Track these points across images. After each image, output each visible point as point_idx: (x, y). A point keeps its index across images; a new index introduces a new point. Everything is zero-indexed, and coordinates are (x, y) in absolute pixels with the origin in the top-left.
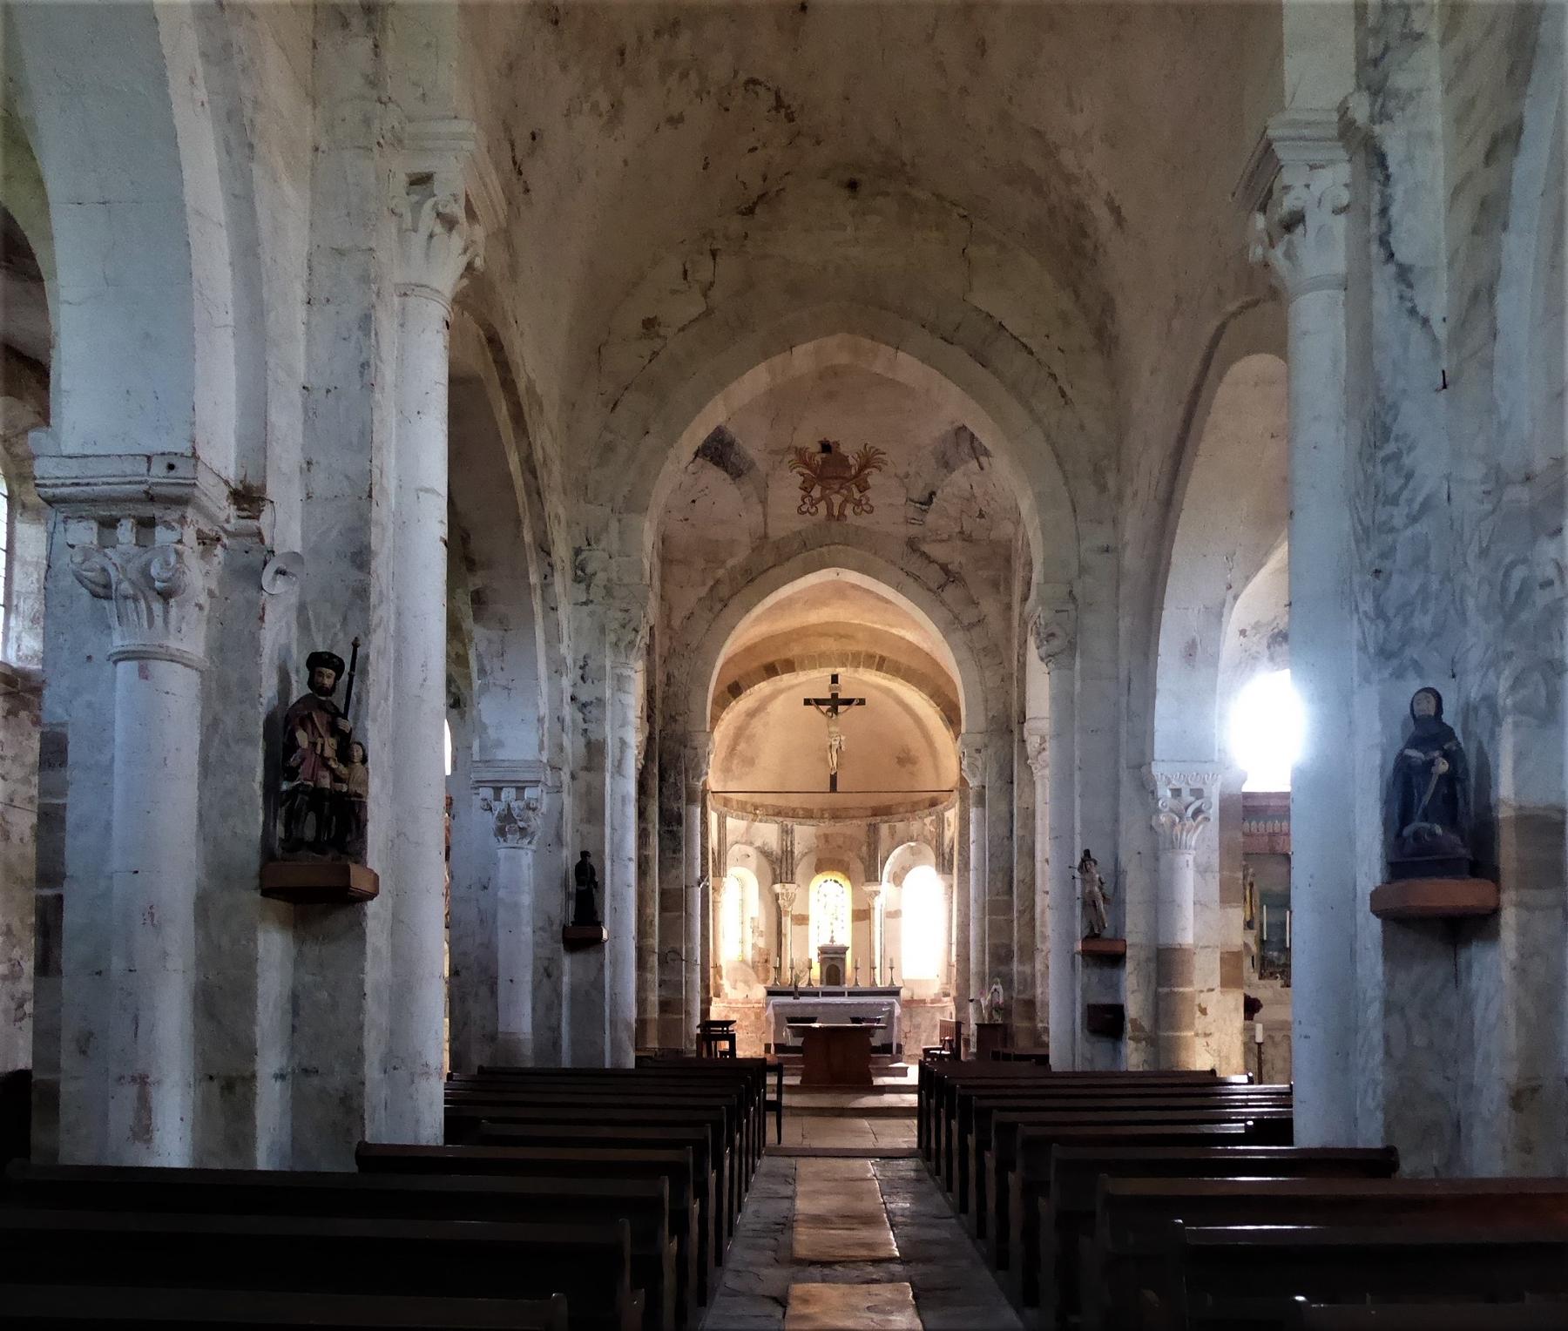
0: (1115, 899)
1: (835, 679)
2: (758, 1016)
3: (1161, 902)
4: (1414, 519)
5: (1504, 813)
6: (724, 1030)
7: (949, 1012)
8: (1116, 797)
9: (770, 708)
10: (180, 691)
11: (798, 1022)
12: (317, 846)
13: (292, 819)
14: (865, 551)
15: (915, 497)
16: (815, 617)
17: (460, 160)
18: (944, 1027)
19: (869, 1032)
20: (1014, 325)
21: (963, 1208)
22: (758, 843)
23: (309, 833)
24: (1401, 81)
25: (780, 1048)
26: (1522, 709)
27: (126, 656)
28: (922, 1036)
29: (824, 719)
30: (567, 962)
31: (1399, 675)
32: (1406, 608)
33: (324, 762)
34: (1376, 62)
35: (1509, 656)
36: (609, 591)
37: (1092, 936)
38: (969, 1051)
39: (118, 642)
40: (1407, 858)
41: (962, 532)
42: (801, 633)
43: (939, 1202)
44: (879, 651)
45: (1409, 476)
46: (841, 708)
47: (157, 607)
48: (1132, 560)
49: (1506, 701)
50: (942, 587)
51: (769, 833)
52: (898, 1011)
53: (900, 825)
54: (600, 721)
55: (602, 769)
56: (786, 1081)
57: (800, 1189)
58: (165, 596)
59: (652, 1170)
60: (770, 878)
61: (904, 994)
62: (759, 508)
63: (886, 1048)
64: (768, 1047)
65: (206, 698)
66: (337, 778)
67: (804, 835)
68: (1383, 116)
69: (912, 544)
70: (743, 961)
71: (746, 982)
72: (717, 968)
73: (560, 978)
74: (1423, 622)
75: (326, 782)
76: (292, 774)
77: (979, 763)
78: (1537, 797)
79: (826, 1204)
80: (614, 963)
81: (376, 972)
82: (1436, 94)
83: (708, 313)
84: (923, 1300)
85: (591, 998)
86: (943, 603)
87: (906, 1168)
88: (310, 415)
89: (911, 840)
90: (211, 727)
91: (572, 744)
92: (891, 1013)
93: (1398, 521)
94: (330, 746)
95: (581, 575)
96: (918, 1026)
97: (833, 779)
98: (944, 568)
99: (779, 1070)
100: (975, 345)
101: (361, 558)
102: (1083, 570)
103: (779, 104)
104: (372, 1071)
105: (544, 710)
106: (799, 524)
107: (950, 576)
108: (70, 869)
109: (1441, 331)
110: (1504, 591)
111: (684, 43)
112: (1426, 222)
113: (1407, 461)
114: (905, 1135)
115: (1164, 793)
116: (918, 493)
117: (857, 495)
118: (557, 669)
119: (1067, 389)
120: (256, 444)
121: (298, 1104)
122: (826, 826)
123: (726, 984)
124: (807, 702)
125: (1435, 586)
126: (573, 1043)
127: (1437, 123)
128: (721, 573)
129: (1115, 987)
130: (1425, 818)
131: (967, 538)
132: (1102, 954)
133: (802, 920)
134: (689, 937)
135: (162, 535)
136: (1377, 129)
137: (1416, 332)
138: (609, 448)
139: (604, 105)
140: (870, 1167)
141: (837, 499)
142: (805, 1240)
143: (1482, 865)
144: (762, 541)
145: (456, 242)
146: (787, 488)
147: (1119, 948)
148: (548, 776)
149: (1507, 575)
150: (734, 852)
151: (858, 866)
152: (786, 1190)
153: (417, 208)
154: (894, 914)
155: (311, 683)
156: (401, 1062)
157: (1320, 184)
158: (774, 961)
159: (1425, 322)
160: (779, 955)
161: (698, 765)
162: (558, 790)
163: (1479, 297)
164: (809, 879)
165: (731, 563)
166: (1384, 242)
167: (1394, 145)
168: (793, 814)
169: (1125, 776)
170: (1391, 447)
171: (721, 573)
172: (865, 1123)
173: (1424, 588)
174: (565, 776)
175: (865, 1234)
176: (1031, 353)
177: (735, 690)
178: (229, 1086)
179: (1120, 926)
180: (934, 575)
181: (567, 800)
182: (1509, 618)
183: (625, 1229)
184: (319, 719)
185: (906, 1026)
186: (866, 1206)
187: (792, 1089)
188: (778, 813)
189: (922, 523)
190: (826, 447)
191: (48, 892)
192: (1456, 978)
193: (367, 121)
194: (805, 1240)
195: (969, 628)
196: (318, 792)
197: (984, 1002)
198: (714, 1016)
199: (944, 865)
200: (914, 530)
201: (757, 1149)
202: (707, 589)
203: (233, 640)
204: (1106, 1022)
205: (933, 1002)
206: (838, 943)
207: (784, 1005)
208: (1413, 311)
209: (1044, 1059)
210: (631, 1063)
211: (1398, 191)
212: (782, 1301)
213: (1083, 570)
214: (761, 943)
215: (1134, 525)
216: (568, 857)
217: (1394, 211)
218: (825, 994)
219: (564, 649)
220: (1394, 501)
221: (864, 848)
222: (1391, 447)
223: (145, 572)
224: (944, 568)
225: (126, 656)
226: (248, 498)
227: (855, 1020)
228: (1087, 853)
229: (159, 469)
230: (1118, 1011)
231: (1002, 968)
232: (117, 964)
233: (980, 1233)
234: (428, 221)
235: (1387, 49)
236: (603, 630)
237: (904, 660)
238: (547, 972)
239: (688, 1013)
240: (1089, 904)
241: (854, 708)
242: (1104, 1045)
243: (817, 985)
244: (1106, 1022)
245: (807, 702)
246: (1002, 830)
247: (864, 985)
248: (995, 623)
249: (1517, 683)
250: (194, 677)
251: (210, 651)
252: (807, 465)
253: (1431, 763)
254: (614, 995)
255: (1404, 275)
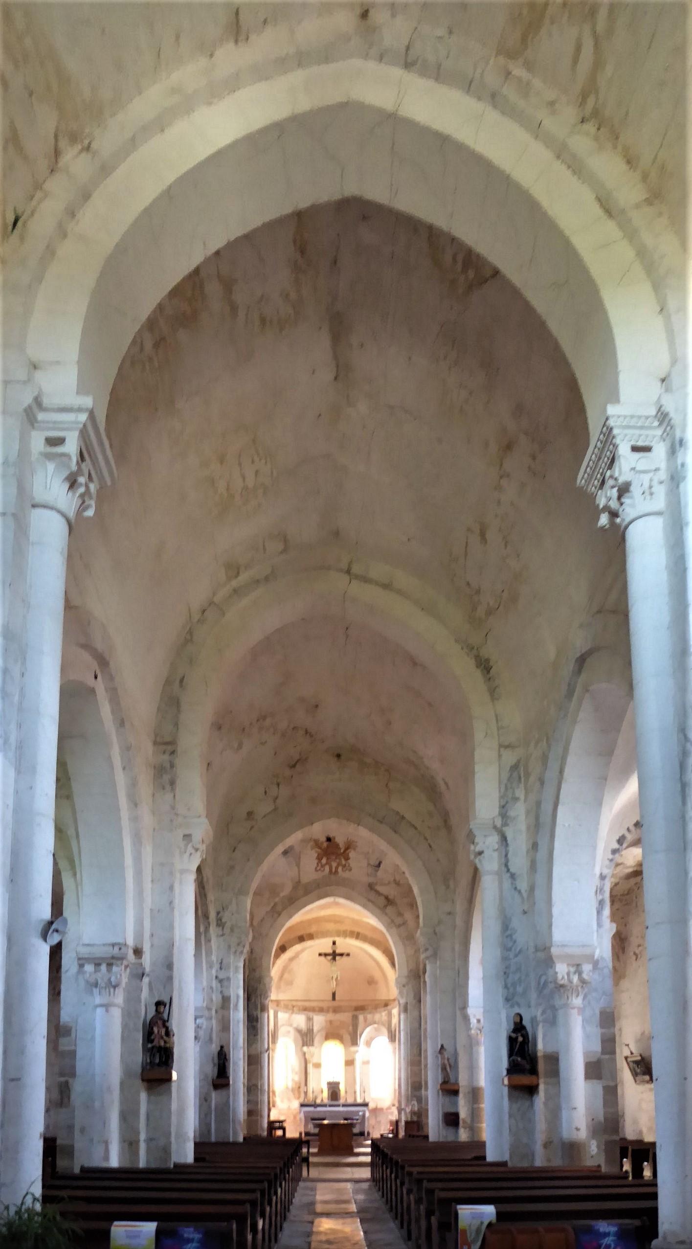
0: (455, 1066)
1: (334, 943)
2: (295, 1117)
3: (472, 1068)
4: (516, 956)
5: (540, 1054)
6: (279, 1125)
7: (394, 1116)
8: (455, 1020)
9: (300, 956)
10: (117, 1014)
11: (314, 1119)
12: (159, 1065)
13: (152, 1056)
14: (348, 889)
15: (372, 863)
16: (323, 913)
17: (202, 830)
18: (391, 1123)
19: (351, 1126)
20: (408, 816)
21: (383, 1196)
22: (295, 1025)
23: (157, 1061)
24: (512, 813)
25: (307, 1134)
26: (545, 1021)
27: (101, 1006)
28: (380, 1129)
29: (329, 964)
30: (214, 1094)
31: (512, 1006)
32: (514, 985)
33: (162, 1038)
34: (503, 807)
35: (540, 1005)
36: (232, 930)
37: (445, 1082)
38: (402, 1133)
39: (98, 1000)
40: (513, 1069)
41: (395, 880)
42: (317, 920)
43: (377, 1195)
44: (357, 930)
45: (515, 942)
46: (337, 958)
47: (112, 990)
48: (459, 921)
49: (539, 1018)
50: (385, 906)
51: (300, 1020)
52: (367, 1114)
53: (369, 1016)
54: (228, 987)
55: (229, 1009)
56: (311, 1150)
57: (319, 1198)
58: (115, 987)
59: (228, 1218)
60: (301, 1042)
61: (372, 1105)
62: (296, 868)
63: (362, 1134)
64: (301, 1134)
65: (123, 1016)
66: (165, 1042)
67: (319, 1021)
68: (505, 824)
69: (371, 886)
70: (287, 1088)
71: (289, 1100)
72: (274, 1093)
73: (211, 1101)
74: (520, 989)
75: (162, 1044)
76: (152, 1041)
77: (405, 991)
78: (550, 1049)
79: (328, 1197)
80: (234, 1095)
81: (174, 1106)
82: (522, 817)
83: (276, 809)
84: (362, 1221)
85: (224, 1111)
86: (386, 914)
87: (365, 1186)
88: (152, 918)
89: (375, 1023)
90: (125, 1027)
91: (216, 998)
92: (364, 1116)
93: (511, 956)
94: (163, 1031)
95: (220, 923)
96: (379, 1122)
97: (334, 995)
98: (387, 898)
99: (308, 1143)
100: (393, 824)
101: (170, 966)
102: (440, 922)
103: (306, 732)
104: (173, 1139)
105: (205, 983)
106: (318, 875)
107: (389, 901)
108: (77, 1074)
109: (525, 895)
110: (539, 983)
111: (268, 722)
112: (519, 862)
113: (514, 937)
114: (366, 1173)
115: (473, 1021)
116: (374, 862)
117: (343, 862)
118: (210, 967)
119: (432, 844)
120: (139, 935)
121: (148, 1150)
122: (331, 1016)
123: (278, 1100)
124: (320, 955)
125: (523, 978)
126: (216, 1130)
127: (523, 827)
128: (277, 900)
129: (456, 1104)
130: (516, 1055)
131: (397, 883)
132: (450, 1090)
133: (318, 1066)
134: (262, 1077)
135: (115, 969)
136: (504, 829)
137: (516, 894)
138: (232, 867)
139: (236, 745)
140: (349, 1185)
141: (334, 865)
142: (319, 1208)
143: (534, 1071)
144: (297, 884)
145: (199, 853)
146: (310, 859)
147: (456, 1088)
148: (206, 1013)
149: (540, 978)
150: (282, 1031)
151: (347, 1037)
152: (313, 1193)
153: (186, 846)
154: (367, 1063)
155: (156, 1010)
156: (181, 1136)
157: (488, 842)
158: (303, 1089)
159: (520, 892)
160: (306, 1084)
161: (266, 992)
162: (211, 1018)
163: (532, 889)
164: (321, 1044)
165: (282, 895)
166: (506, 865)
167: (509, 832)
168: (313, 1010)
169: (458, 1013)
170: (509, 932)
171: (277, 900)
172: (349, 1169)
173: (520, 979)
174: (213, 1012)
175: (343, 1206)
176: (416, 828)
177: (283, 949)
178: (131, 1144)
179: (457, 1079)
180: (382, 901)
181: (214, 1022)
182: (541, 992)
183: (248, 1207)
184: (160, 1023)
185: (372, 1122)
186: (345, 1197)
187: (314, 1155)
188: (305, 1009)
189: (376, 876)
190: (329, 839)
191: (63, 1079)
192: (532, 1105)
193: (171, 821)
194: (319, 1208)
195: (399, 926)
196: (160, 1047)
197: (408, 1110)
198: (272, 1118)
199: (392, 1038)
200: (371, 880)
201: (298, 1179)
202: (270, 907)
203: (132, 998)
204: (452, 1120)
205: (387, 1109)
206: (336, 1080)
207: (309, 1112)
208: (516, 889)
209: (427, 1137)
210: (241, 1139)
211: (511, 849)
212: (312, 1223)
213: (440, 922)
214: (297, 1078)
215: (459, 908)
216: (215, 1048)
217: (509, 856)
218: (330, 1106)
219: (214, 958)
220: (510, 949)
221: (351, 1028)
222: (509, 932)
223: (109, 980)
224: (387, 898)
225: (101, 1006)
226: (138, 952)
227: (346, 1119)
228: (442, 1046)
229: (116, 948)
230: (456, 1116)
231: (417, 1093)
232: (97, 1104)
233: (391, 1209)
234: (190, 849)
235: (507, 802)
236: (229, 947)
237: (369, 934)
238: (204, 1100)
239: (261, 1116)
240: (444, 1069)
241: (345, 958)
242: (451, 1130)
243: (326, 1101)
244: (452, 1120)
245: (320, 955)
246: (417, 1025)
247: (350, 1101)
248: (411, 923)
249: (544, 1012)
250: (120, 1010)
251: (124, 1001)
252: (320, 848)
253: (517, 1038)
254: (234, 1109)
255: (513, 876)
